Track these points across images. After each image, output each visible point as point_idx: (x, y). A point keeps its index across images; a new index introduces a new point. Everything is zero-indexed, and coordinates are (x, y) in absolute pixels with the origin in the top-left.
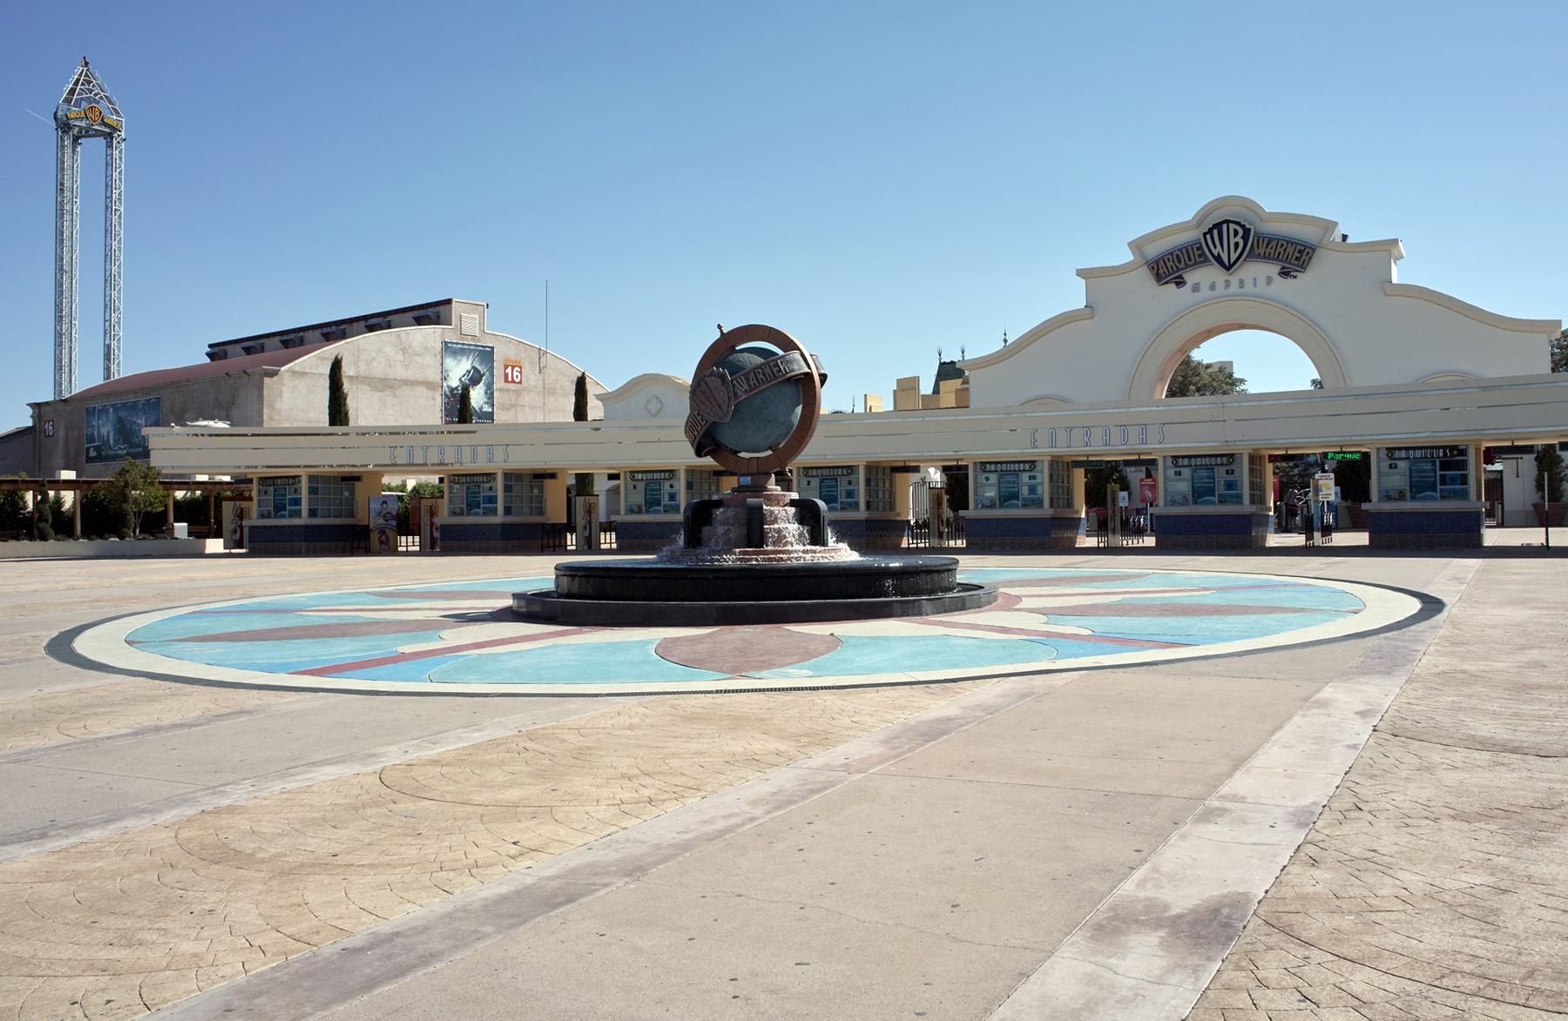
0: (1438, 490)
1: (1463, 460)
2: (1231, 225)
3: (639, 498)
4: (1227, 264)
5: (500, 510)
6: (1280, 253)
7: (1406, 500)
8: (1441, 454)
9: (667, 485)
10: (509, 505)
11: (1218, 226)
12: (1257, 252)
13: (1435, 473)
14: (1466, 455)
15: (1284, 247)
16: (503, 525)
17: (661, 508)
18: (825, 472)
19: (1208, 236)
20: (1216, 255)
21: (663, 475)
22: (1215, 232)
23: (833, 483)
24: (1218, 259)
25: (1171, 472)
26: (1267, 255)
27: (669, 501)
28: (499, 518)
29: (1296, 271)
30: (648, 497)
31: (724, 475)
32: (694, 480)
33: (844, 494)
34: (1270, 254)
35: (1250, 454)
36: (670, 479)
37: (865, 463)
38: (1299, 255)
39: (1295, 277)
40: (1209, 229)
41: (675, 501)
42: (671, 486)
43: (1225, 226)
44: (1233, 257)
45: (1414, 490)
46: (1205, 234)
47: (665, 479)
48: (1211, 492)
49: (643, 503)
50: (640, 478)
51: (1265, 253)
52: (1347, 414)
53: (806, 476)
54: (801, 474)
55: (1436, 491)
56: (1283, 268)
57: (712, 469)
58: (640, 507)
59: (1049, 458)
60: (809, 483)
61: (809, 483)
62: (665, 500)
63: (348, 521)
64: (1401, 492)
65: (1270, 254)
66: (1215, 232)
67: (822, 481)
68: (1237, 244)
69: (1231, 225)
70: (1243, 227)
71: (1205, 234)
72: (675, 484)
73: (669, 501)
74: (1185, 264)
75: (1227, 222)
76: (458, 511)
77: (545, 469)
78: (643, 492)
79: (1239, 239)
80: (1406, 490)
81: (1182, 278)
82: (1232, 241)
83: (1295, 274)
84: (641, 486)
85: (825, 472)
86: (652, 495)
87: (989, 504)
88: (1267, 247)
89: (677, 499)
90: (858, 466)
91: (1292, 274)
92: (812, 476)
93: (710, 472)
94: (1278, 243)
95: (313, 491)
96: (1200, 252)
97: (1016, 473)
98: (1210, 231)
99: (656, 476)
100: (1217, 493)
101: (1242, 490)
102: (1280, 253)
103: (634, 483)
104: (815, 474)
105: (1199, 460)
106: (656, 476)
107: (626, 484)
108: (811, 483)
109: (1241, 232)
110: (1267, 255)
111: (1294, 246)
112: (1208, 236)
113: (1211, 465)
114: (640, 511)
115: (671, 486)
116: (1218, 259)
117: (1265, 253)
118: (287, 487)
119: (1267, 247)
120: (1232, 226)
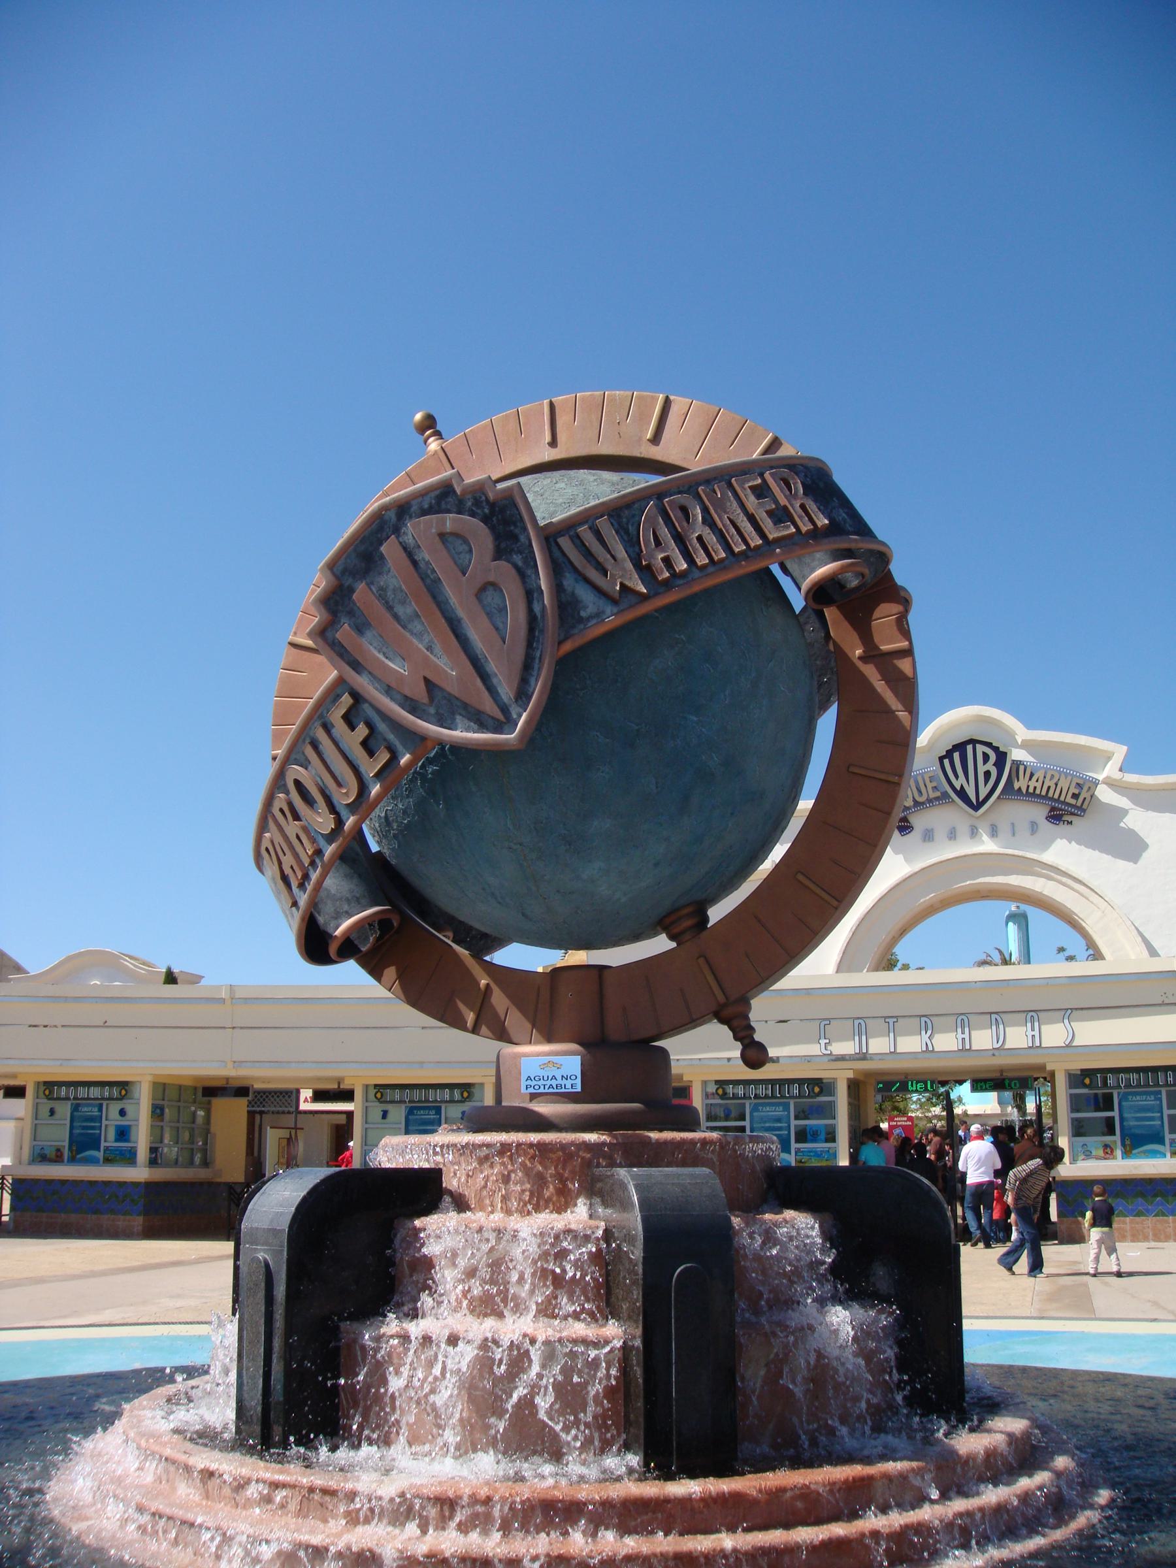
0: (1167, 1141)
1: (831, 1102)
2: (978, 746)
3: (59, 1134)
4: (974, 801)
5: (142, 1154)
6: (1049, 788)
7: (62, 1161)
8: (796, 1092)
9: (114, 1108)
10: (157, 1145)
11: (960, 747)
12: (1016, 785)
13: (1161, 1112)
14: (1071, 1095)
15: (1055, 780)
16: (150, 1187)
17: (100, 1155)
18: (417, 1095)
19: (946, 762)
20: (958, 788)
21: (447, 1094)
22: (956, 756)
23: (432, 1116)
24: (962, 794)
25: (376, 1113)
26: (1031, 790)
27: (117, 1140)
28: (139, 1173)
29: (1072, 814)
30: (77, 1131)
31: (223, 1095)
32: (165, 1103)
33: (112, 1134)
34: (1035, 788)
35: (849, 1080)
36: (121, 1098)
37: (851, 1075)
38: (1077, 792)
39: (1070, 823)
40: (947, 751)
41: (128, 1141)
42: (122, 1113)
43: (970, 748)
44: (983, 793)
45: (1128, 1142)
46: (941, 759)
47: (111, 1099)
48: (94, 1143)
49: (66, 1144)
50: (63, 1094)
51: (1028, 786)
52: (241, 1028)
53: (381, 1100)
54: (41, 1093)
55: (789, 1153)
56: (1053, 809)
57: (200, 1085)
58: (59, 1151)
59: (150, 1078)
60: (385, 1115)
61: (385, 1115)
62: (109, 1139)
63: (200, 1174)
64: (58, 1150)
65: (1035, 788)
66: (956, 756)
67: (411, 1111)
68: (987, 774)
69: (978, 746)
70: (996, 749)
71: (941, 759)
72: (130, 1109)
73: (117, 1140)
74: (914, 800)
75: (973, 742)
76: (50, 1152)
77: (227, 1079)
78: (68, 1122)
79: (990, 766)
80: (64, 1146)
81: (908, 821)
82: (982, 769)
83: (1069, 818)
84: (64, 1110)
85: (417, 1095)
86: (84, 1128)
87: (53, 1156)
88: (1030, 779)
89: (133, 1138)
90: (482, 1084)
91: (1065, 818)
92: (59, 1099)
93: (195, 1088)
94: (1045, 773)
95: (157, 1111)
96: (934, 784)
97: (99, 1103)
98: (949, 754)
99: (95, 1092)
100: (103, 1144)
101: (137, 1142)
102: (1049, 788)
103: (51, 1104)
104: (397, 1097)
105: (81, 1090)
106: (95, 1092)
107: (366, 1110)
108: (390, 1116)
109: (993, 757)
110: (1031, 790)
111: (1069, 778)
112: (946, 762)
113: (436, 1101)
114: (57, 1158)
115: (122, 1113)
116: (962, 794)
117: (1028, 786)
118: (105, 1103)
119: (1030, 779)
120: (980, 749)
